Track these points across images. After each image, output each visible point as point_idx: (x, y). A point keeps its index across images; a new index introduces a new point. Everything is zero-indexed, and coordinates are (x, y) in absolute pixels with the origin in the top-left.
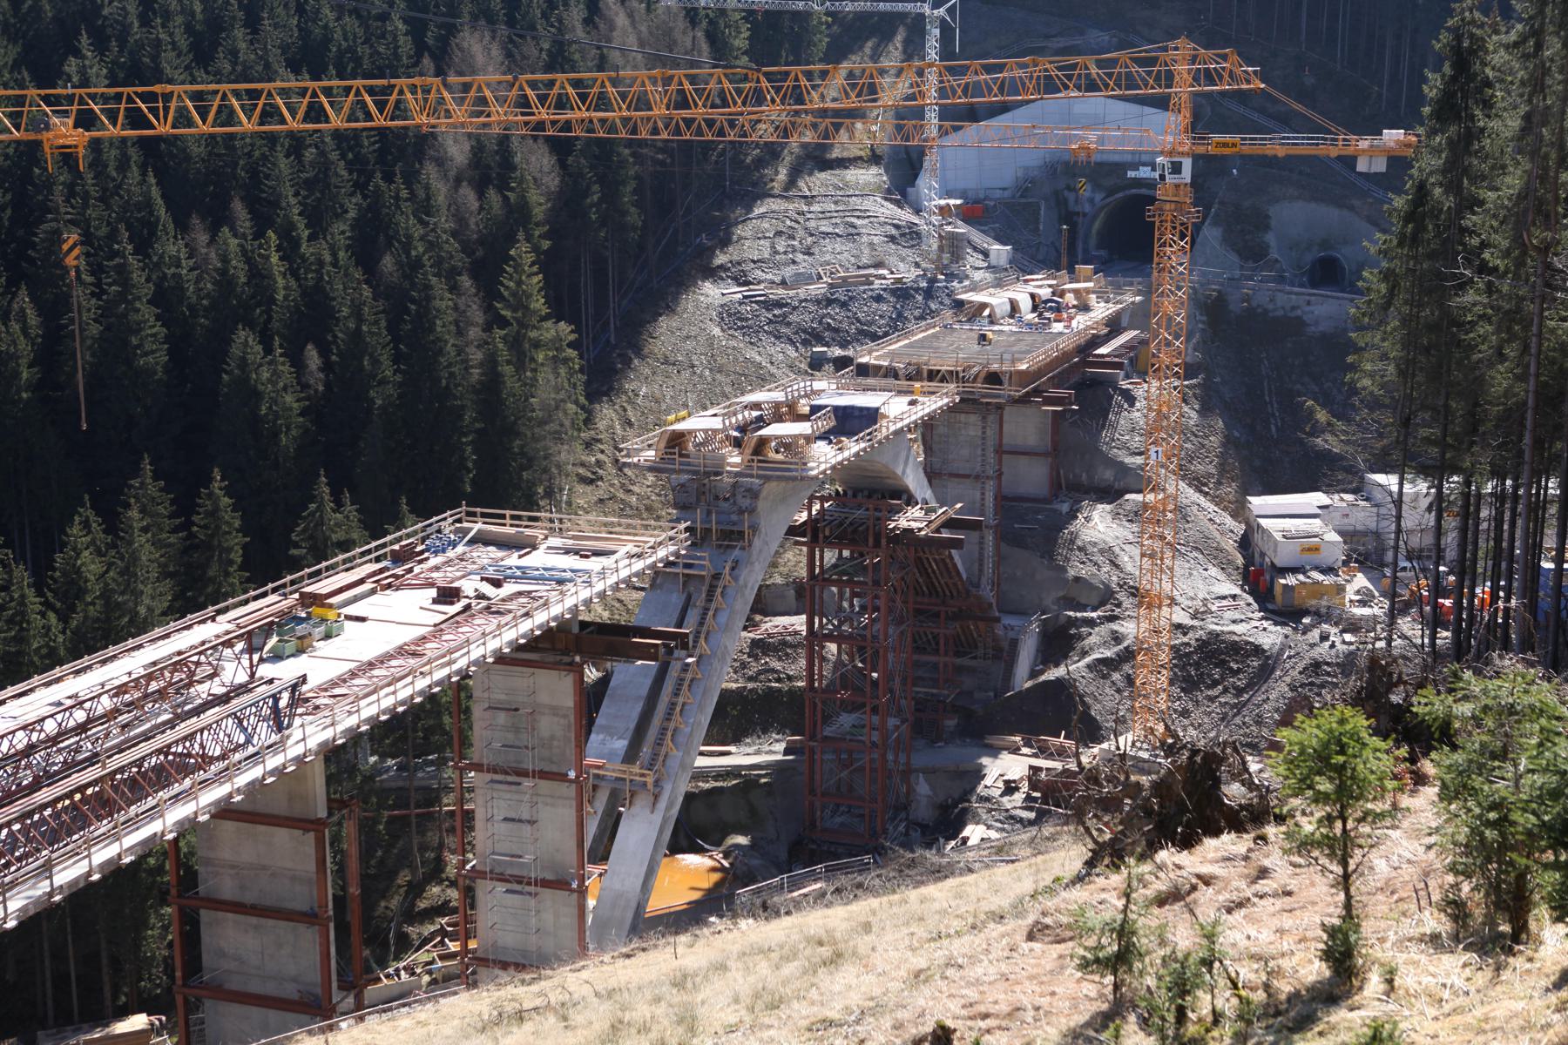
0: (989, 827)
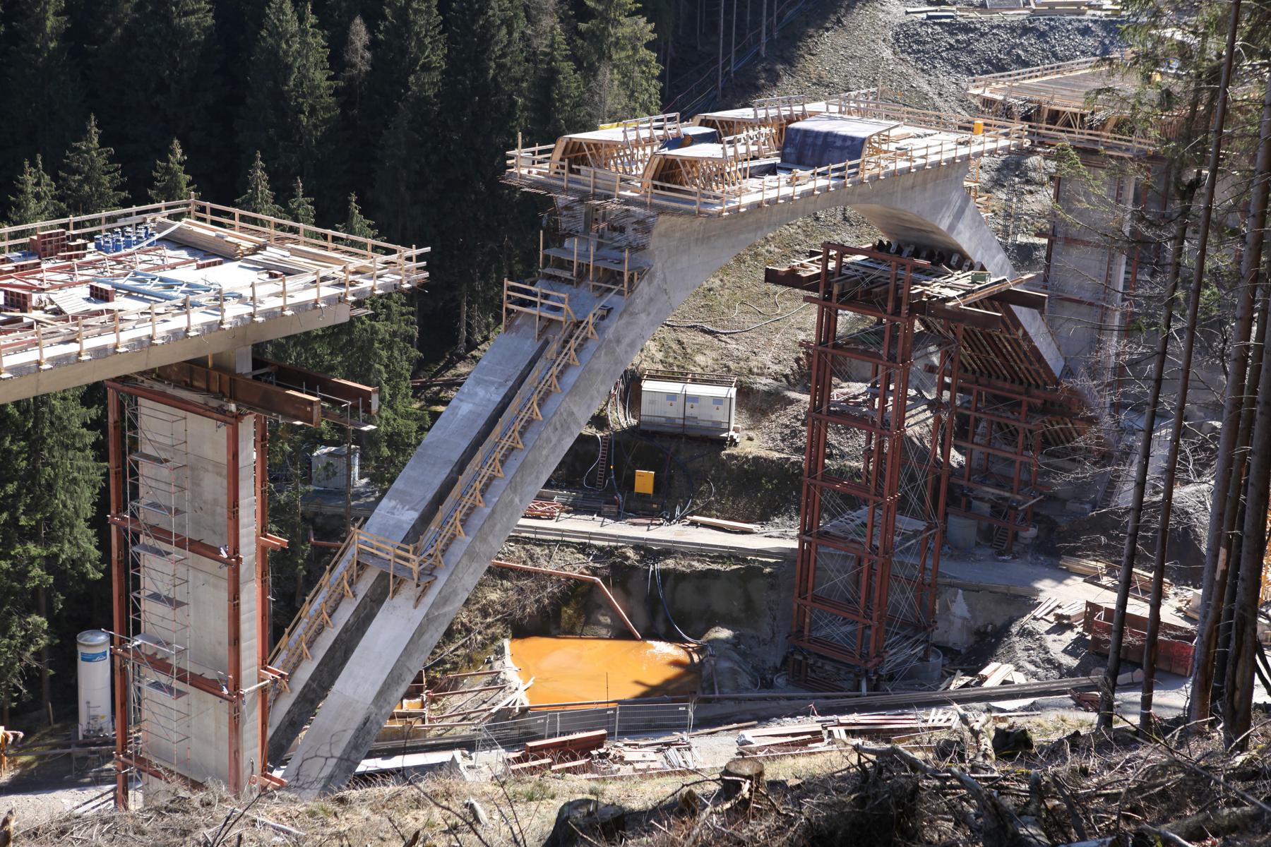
0: (1019, 668)
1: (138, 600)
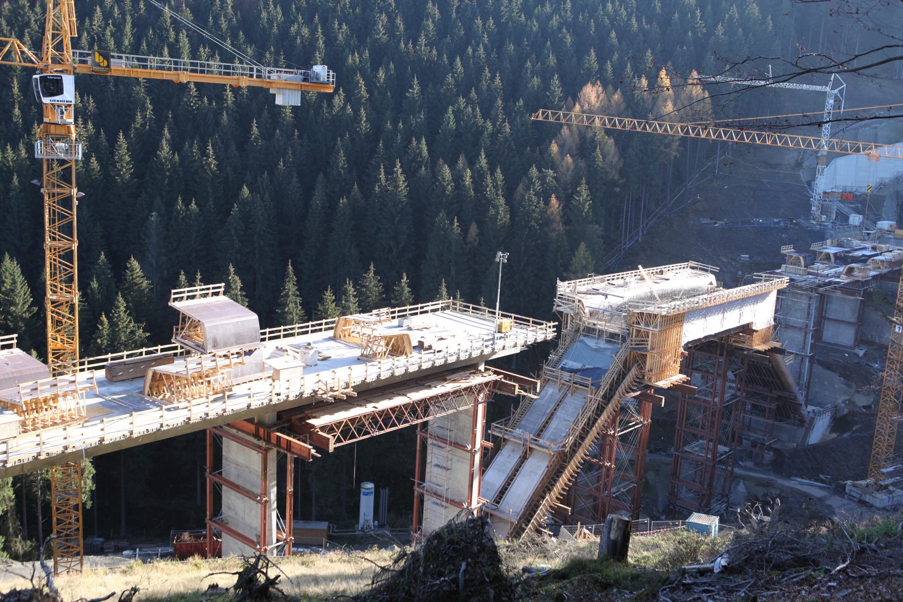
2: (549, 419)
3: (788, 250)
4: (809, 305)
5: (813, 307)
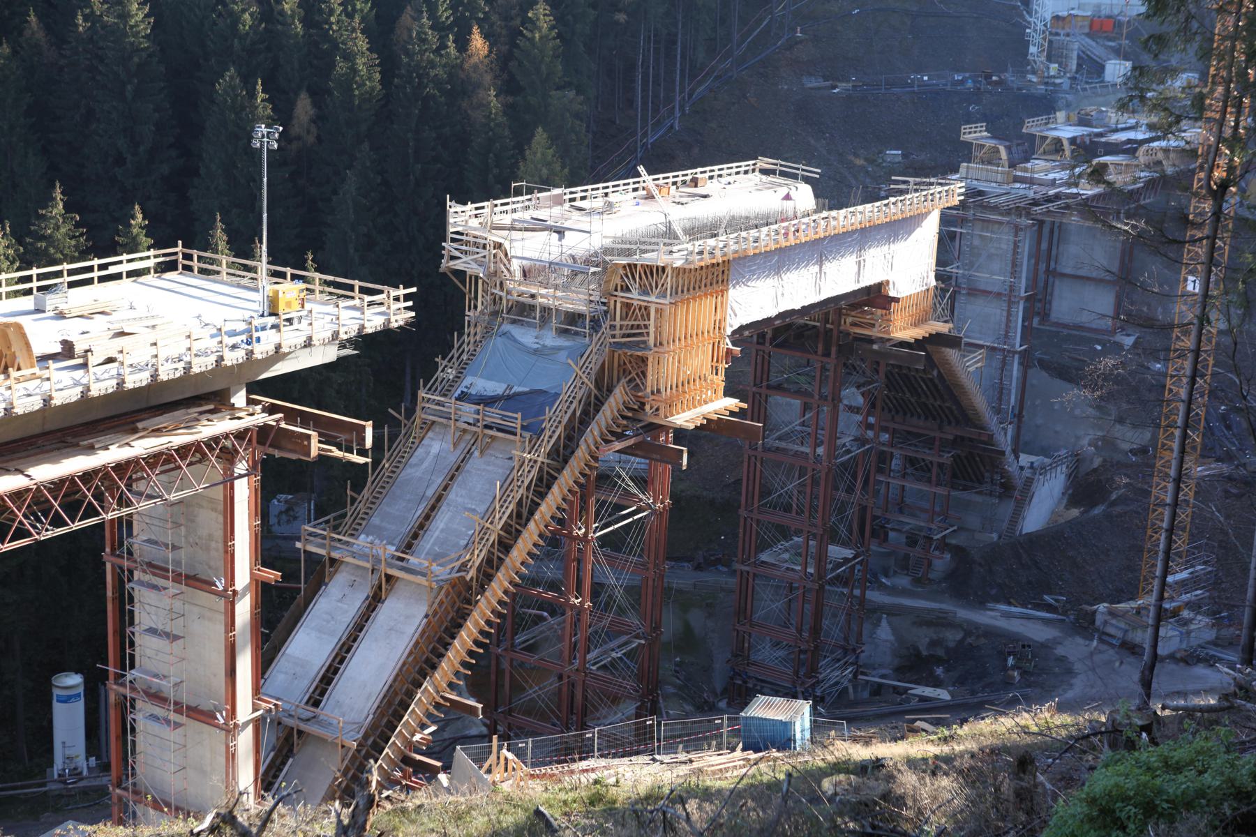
1: (133, 634)
2: (433, 508)
3: (975, 134)
4: (1016, 245)
5: (1025, 248)
